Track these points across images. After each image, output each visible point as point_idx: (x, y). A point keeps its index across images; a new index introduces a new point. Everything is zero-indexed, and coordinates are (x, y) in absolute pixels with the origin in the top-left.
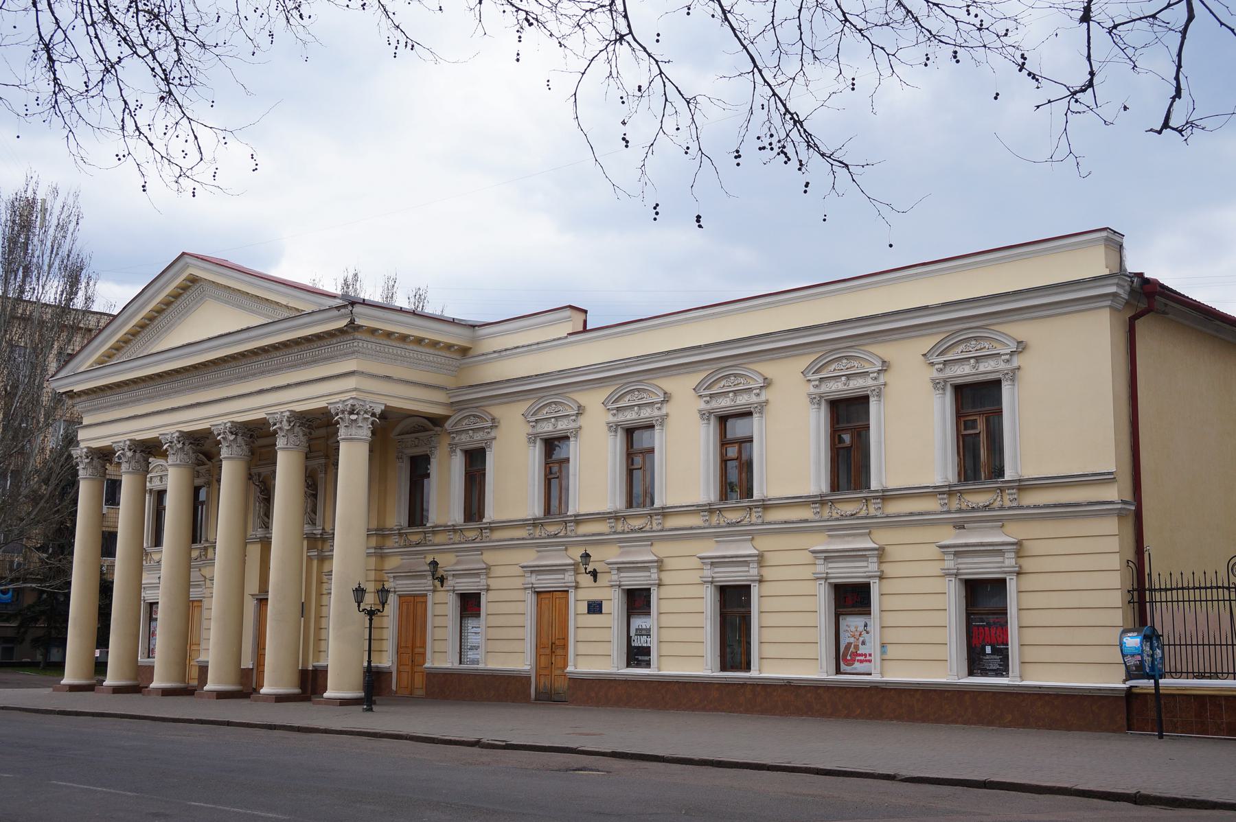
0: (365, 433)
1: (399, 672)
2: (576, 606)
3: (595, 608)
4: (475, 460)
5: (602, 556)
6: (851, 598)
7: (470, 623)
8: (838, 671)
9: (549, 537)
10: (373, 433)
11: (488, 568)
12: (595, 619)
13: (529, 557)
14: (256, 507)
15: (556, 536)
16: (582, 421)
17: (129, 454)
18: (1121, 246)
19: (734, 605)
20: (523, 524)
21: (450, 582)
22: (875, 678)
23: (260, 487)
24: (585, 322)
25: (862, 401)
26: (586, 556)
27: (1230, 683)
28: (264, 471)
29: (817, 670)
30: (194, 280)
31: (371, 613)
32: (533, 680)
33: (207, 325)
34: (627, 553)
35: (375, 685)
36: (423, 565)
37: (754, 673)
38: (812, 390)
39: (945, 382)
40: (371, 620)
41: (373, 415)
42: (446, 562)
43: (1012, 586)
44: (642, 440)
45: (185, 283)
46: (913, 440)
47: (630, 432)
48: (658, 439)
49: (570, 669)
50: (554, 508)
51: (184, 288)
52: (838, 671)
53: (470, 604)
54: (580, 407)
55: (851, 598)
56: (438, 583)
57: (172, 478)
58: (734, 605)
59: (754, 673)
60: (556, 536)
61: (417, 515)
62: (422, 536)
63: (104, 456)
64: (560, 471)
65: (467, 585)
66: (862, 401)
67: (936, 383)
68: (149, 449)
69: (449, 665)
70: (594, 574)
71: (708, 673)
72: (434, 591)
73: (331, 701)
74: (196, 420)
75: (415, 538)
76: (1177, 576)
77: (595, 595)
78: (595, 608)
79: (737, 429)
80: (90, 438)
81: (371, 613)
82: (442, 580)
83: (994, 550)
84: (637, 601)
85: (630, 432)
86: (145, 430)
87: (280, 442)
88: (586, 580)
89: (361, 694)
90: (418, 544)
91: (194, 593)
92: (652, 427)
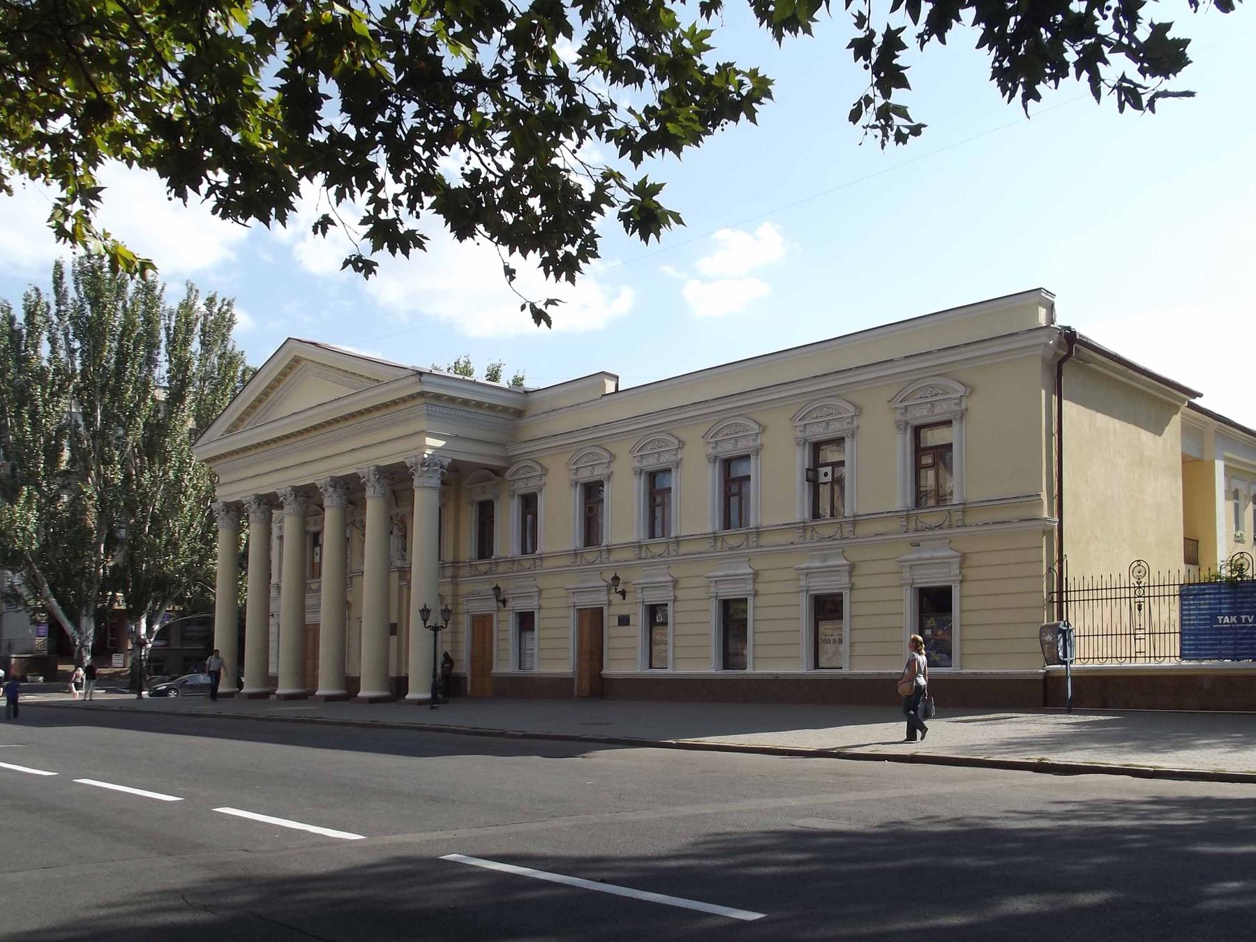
0: (436, 482)
1: (473, 676)
2: (610, 621)
3: (624, 621)
4: (529, 503)
5: (634, 578)
6: (827, 608)
7: (528, 635)
8: (651, 667)
9: (588, 563)
10: (443, 483)
11: (540, 592)
12: (624, 630)
13: (572, 582)
14: (395, 541)
15: (593, 563)
16: (614, 467)
17: (331, 490)
18: (1053, 305)
19: (733, 619)
20: (788, 527)
21: (510, 604)
22: (845, 671)
23: (398, 525)
24: (617, 386)
25: (600, 484)
26: (616, 578)
27: (1247, 663)
28: (401, 511)
29: (799, 667)
30: (297, 360)
31: (436, 629)
32: (576, 681)
33: (308, 399)
34: (584, 581)
35: (448, 686)
36: (487, 588)
37: (749, 670)
38: (799, 434)
39: (716, 457)
40: (436, 635)
41: (442, 467)
42: (508, 587)
43: (670, 610)
44: (739, 470)
45: (296, 360)
46: (778, 491)
47: (727, 463)
48: (674, 481)
49: (605, 671)
50: (529, 549)
51: (290, 367)
52: (817, 666)
53: (526, 621)
54: (611, 455)
55: (827, 608)
56: (501, 605)
57: (287, 523)
58: (733, 619)
59: (749, 670)
60: (940, 527)
61: (485, 548)
62: (597, 554)
63: (237, 510)
64: (740, 489)
65: (523, 605)
66: (600, 484)
67: (898, 425)
68: (270, 502)
69: (510, 671)
70: (623, 593)
71: (713, 671)
72: (498, 610)
73: (412, 702)
74: (303, 477)
75: (483, 568)
76: (1115, 576)
77: (624, 612)
78: (624, 621)
79: (739, 470)
80: (225, 494)
81: (436, 629)
82: (504, 602)
83: (739, 579)
84: (655, 614)
85: (727, 463)
86: (266, 486)
87: (369, 492)
88: (616, 598)
89: (428, 696)
90: (485, 573)
91: (310, 619)
92: (842, 439)
